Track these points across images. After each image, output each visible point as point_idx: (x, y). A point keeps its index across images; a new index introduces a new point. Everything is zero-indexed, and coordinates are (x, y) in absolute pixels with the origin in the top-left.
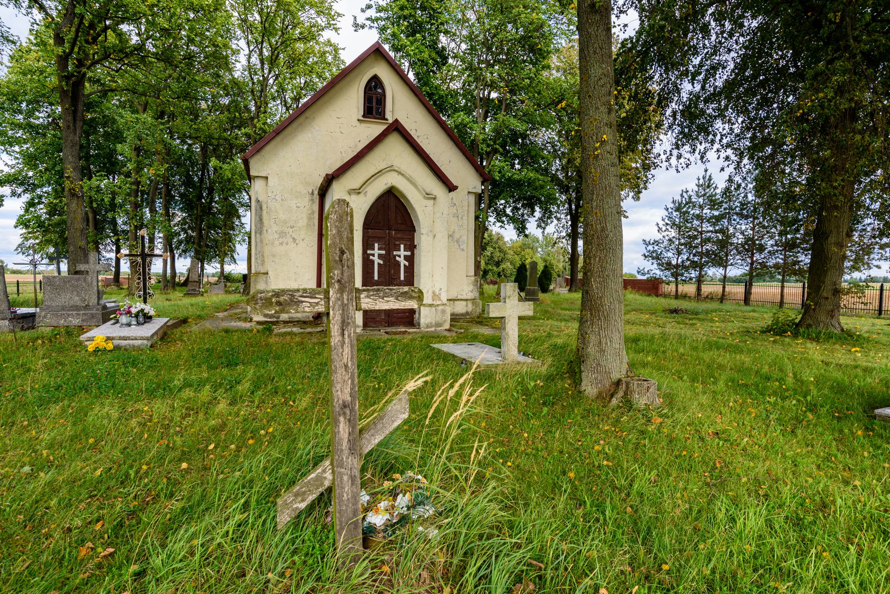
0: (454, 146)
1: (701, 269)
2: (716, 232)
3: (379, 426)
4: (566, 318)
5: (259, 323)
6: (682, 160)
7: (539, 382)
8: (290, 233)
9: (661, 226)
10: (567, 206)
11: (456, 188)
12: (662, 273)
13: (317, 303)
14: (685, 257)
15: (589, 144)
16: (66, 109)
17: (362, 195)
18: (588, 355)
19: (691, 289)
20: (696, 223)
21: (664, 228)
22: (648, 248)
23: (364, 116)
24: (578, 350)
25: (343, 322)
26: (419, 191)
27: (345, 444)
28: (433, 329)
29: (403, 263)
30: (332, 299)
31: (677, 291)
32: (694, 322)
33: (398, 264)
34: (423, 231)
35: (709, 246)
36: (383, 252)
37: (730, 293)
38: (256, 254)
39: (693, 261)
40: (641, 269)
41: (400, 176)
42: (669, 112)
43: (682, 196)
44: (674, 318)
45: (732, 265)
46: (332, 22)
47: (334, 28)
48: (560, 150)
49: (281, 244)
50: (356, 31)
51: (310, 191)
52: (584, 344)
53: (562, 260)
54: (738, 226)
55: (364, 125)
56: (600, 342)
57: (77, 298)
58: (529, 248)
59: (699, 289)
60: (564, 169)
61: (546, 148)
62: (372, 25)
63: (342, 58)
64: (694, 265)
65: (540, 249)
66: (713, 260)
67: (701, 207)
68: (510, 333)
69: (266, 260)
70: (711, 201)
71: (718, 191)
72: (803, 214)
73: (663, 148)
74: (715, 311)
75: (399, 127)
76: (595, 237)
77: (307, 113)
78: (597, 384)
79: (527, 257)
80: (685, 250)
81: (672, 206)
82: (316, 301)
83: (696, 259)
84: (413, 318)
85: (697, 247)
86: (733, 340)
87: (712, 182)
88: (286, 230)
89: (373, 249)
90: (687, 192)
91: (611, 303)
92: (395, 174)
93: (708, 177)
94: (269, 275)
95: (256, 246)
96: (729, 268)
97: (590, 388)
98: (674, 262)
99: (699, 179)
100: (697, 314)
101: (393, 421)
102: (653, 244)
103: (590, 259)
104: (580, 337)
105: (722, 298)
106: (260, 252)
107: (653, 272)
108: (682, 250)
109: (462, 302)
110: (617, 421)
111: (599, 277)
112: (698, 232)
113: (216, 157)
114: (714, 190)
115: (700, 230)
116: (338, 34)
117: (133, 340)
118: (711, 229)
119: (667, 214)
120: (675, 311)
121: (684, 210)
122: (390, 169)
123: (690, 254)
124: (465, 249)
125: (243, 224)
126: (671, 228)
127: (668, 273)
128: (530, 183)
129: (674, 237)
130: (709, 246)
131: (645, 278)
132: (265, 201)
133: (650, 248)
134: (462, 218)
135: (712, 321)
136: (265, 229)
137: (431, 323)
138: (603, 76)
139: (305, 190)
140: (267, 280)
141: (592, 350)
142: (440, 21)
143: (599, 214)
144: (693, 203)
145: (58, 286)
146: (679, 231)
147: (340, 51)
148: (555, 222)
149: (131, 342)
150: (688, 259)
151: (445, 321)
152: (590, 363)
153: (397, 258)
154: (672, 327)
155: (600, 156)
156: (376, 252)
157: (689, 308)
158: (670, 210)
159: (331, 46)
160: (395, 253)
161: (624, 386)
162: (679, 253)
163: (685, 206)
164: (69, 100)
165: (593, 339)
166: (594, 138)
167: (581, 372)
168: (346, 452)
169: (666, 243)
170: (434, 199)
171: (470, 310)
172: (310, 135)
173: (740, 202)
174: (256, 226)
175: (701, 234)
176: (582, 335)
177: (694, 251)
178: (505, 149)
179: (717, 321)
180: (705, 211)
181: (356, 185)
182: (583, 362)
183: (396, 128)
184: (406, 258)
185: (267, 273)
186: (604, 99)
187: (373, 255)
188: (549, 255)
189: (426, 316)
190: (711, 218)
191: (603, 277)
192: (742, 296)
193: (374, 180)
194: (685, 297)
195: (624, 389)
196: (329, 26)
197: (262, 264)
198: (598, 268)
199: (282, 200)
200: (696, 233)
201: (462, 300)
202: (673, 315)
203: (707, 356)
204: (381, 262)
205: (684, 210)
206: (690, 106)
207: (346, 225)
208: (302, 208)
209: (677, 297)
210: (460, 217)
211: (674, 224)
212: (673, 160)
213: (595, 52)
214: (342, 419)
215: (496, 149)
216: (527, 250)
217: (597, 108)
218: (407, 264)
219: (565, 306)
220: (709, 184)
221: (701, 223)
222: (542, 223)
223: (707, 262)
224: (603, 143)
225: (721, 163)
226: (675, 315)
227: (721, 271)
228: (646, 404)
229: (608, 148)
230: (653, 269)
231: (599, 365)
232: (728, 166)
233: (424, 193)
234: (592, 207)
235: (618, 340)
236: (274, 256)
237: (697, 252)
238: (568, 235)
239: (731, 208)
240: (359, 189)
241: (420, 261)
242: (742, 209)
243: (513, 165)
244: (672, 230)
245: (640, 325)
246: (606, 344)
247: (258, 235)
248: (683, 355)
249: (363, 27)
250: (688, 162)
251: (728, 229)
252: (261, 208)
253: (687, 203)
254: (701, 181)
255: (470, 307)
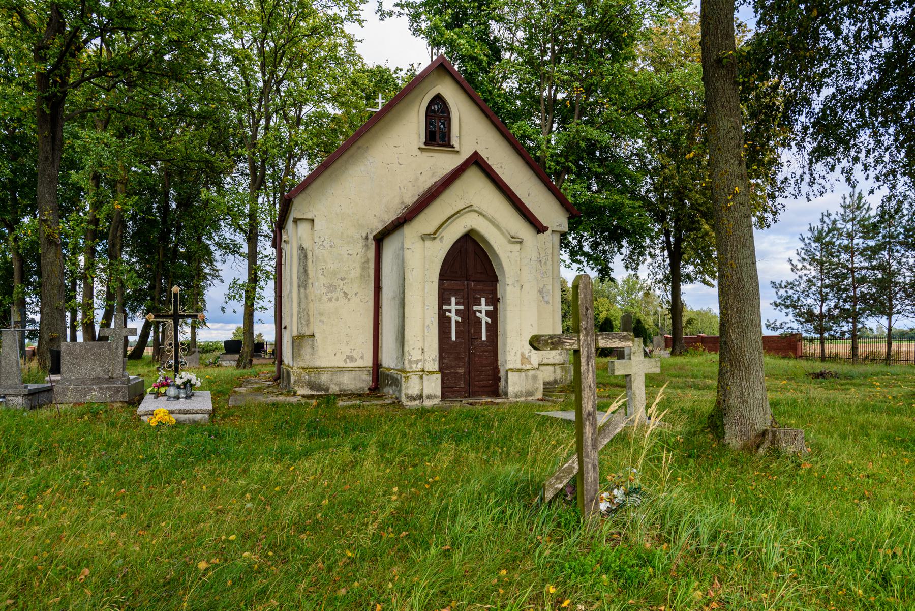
0: (534, 175)
1: (856, 321)
2: (873, 268)
3: (607, 432)
4: (681, 385)
5: (304, 396)
6: (816, 187)
7: (678, 437)
8: (341, 286)
9: (795, 262)
10: (662, 238)
11: (546, 229)
12: (800, 326)
13: (574, 343)
14: (832, 304)
15: (721, 195)
16: (45, 137)
17: (437, 240)
18: (730, 407)
19: (842, 348)
20: (844, 257)
21: (800, 266)
22: (780, 293)
23: (426, 143)
24: (719, 403)
25: (588, 356)
26: (503, 233)
27: (589, 442)
28: (523, 399)
29: (485, 320)
30: (582, 341)
31: (823, 350)
32: (847, 387)
33: (479, 321)
34: (509, 281)
35: (864, 289)
36: (461, 307)
37: (898, 353)
38: (299, 313)
39: (844, 310)
40: (771, 322)
41: (481, 217)
42: (798, 127)
43: (822, 221)
44: (821, 383)
45: (898, 312)
46: (355, 12)
47: (356, 20)
48: (651, 164)
49: (330, 300)
50: (382, 19)
51: (364, 235)
52: (726, 396)
53: (651, 313)
54: (904, 260)
55: (425, 154)
56: (742, 394)
57: (99, 369)
58: (603, 296)
59: (854, 348)
60: (658, 189)
61: (631, 162)
62: (402, 11)
64: (847, 315)
65: (619, 298)
66: (872, 306)
67: (850, 236)
68: (637, 392)
69: (311, 320)
70: (864, 227)
71: (873, 213)
73: (791, 169)
74: (877, 374)
75: (480, 161)
76: (732, 287)
77: (361, 143)
78: (741, 436)
79: (601, 309)
80: (831, 294)
81: (810, 234)
82: (573, 341)
83: (847, 306)
84: (498, 386)
85: (848, 290)
86: (895, 404)
87: (863, 201)
88: (335, 282)
89: (450, 304)
90: (829, 215)
91: (751, 353)
92: (475, 215)
93: (856, 195)
94: (316, 338)
95: (300, 303)
96: (894, 317)
97: (734, 441)
98: (817, 311)
99: (845, 198)
100: (852, 377)
101: (616, 429)
102: (786, 287)
103: (727, 309)
104: (720, 389)
105: (889, 358)
106: (304, 310)
107: (788, 325)
108: (827, 293)
109: (548, 367)
110: (767, 467)
111: (738, 327)
112: (848, 269)
114: (867, 211)
115: (850, 266)
116: (362, 27)
117: (193, 413)
118: (866, 264)
119: (803, 246)
120: (822, 375)
121: (827, 239)
122: (469, 209)
123: (839, 300)
124: (551, 302)
125: (217, 271)
126: (810, 264)
127: (809, 326)
128: (615, 209)
129: (814, 277)
130: (864, 289)
131: (777, 333)
132: (310, 248)
133: (782, 292)
134: (545, 263)
135: (872, 385)
136: (310, 281)
137: (521, 392)
138: (732, 129)
139: (359, 234)
140: (313, 344)
141: (734, 401)
142: (492, 6)
143: (734, 266)
144: (838, 230)
145: (78, 354)
146: (822, 270)
147: (356, 44)
148: (649, 260)
149: (191, 416)
150: (836, 307)
151: (537, 389)
152: (733, 415)
153: (478, 314)
154: (818, 392)
155: (733, 208)
156: (454, 307)
157: (839, 372)
158: (807, 241)
159: (345, 37)
160: (475, 308)
161: (770, 435)
162: (824, 299)
163: (827, 234)
164: (49, 126)
165: (735, 390)
166: (726, 190)
167: (723, 425)
168: (590, 448)
169: (803, 285)
170: (521, 242)
171: (558, 377)
172: (363, 169)
173: (904, 227)
174: (299, 278)
175: (853, 272)
176: (722, 387)
177: (844, 295)
178: (578, 166)
179: (878, 386)
180: (855, 241)
181: (431, 229)
182: (725, 414)
183: (476, 161)
184: (488, 314)
185: (313, 336)
186: (734, 152)
187: (450, 311)
188: (632, 305)
189: (515, 384)
190: (865, 250)
191: (742, 328)
193: (451, 223)
194: (835, 358)
195: (770, 438)
196: (351, 17)
197: (307, 325)
198: (736, 319)
199: (331, 246)
200: (845, 271)
201: (548, 365)
202: (818, 380)
203: (861, 419)
204: (459, 319)
205: (827, 239)
206: (824, 117)
207: (589, 291)
208: (354, 256)
209: (823, 358)
210: (543, 262)
211: (813, 259)
212: (805, 187)
213: (723, 106)
214: (587, 423)
215: (569, 167)
216: (601, 300)
217: (727, 161)
218: (489, 320)
219: (674, 372)
220: (858, 205)
221: (852, 257)
222: (632, 263)
223: (864, 310)
224: (735, 195)
225: (871, 183)
226: (821, 379)
227: (884, 321)
228: (794, 452)
229: (740, 199)
230: (789, 322)
231: (742, 416)
232: (879, 187)
233: (509, 236)
234: (727, 259)
235: (761, 391)
236: (321, 314)
237: (848, 296)
238: (666, 277)
239: (891, 236)
240: (435, 233)
241: (505, 317)
242: (906, 237)
243: (589, 188)
244: (812, 268)
245: (777, 391)
246: (749, 394)
247: (302, 290)
248: (833, 418)
249: (390, 14)
250: (822, 189)
251: (889, 264)
252: (306, 257)
253: (830, 231)
254: (848, 201)
255: (559, 374)
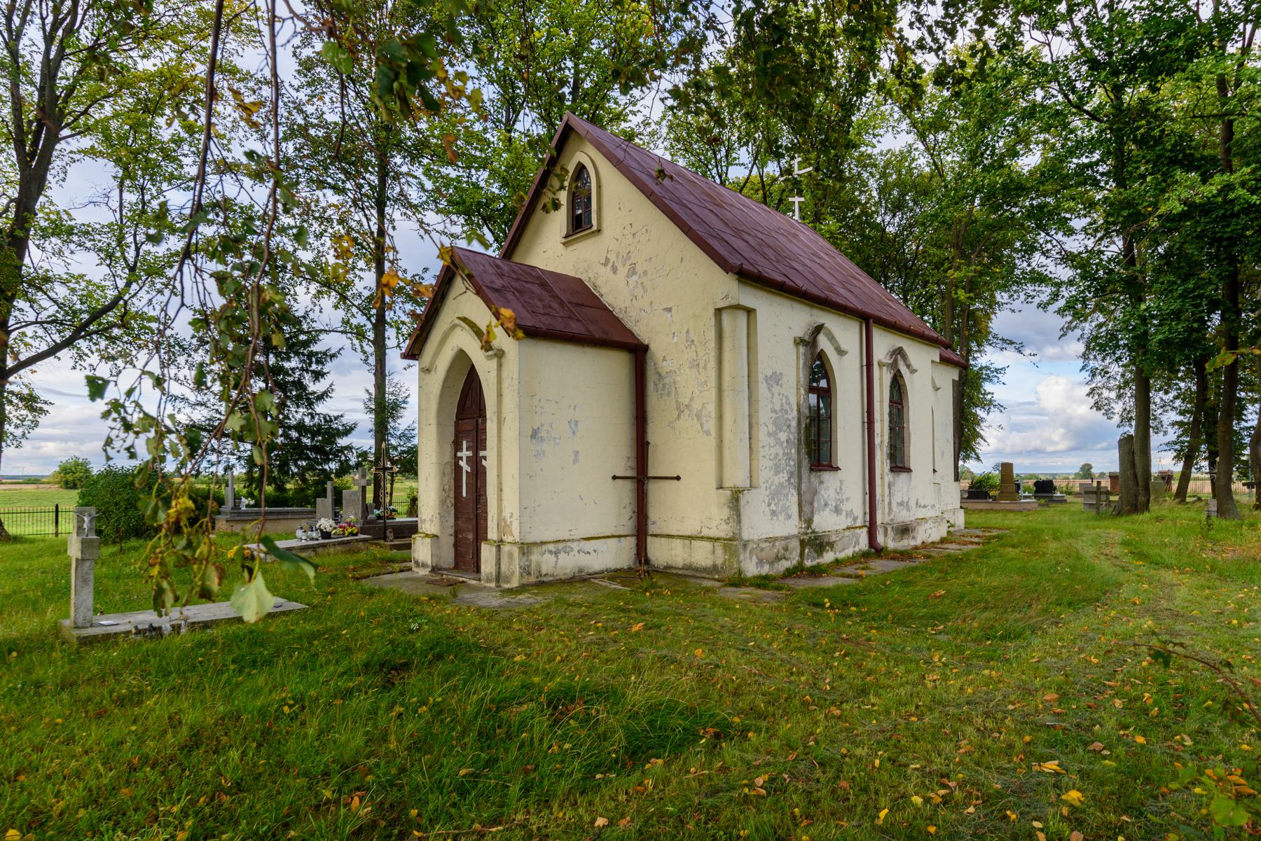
63: (101, 161)
72: (8, 682)
113: (1004, 288)
134: (705, 367)
171: (719, 562)
192: (459, 285)
201: (702, 538)
210: (702, 365)
